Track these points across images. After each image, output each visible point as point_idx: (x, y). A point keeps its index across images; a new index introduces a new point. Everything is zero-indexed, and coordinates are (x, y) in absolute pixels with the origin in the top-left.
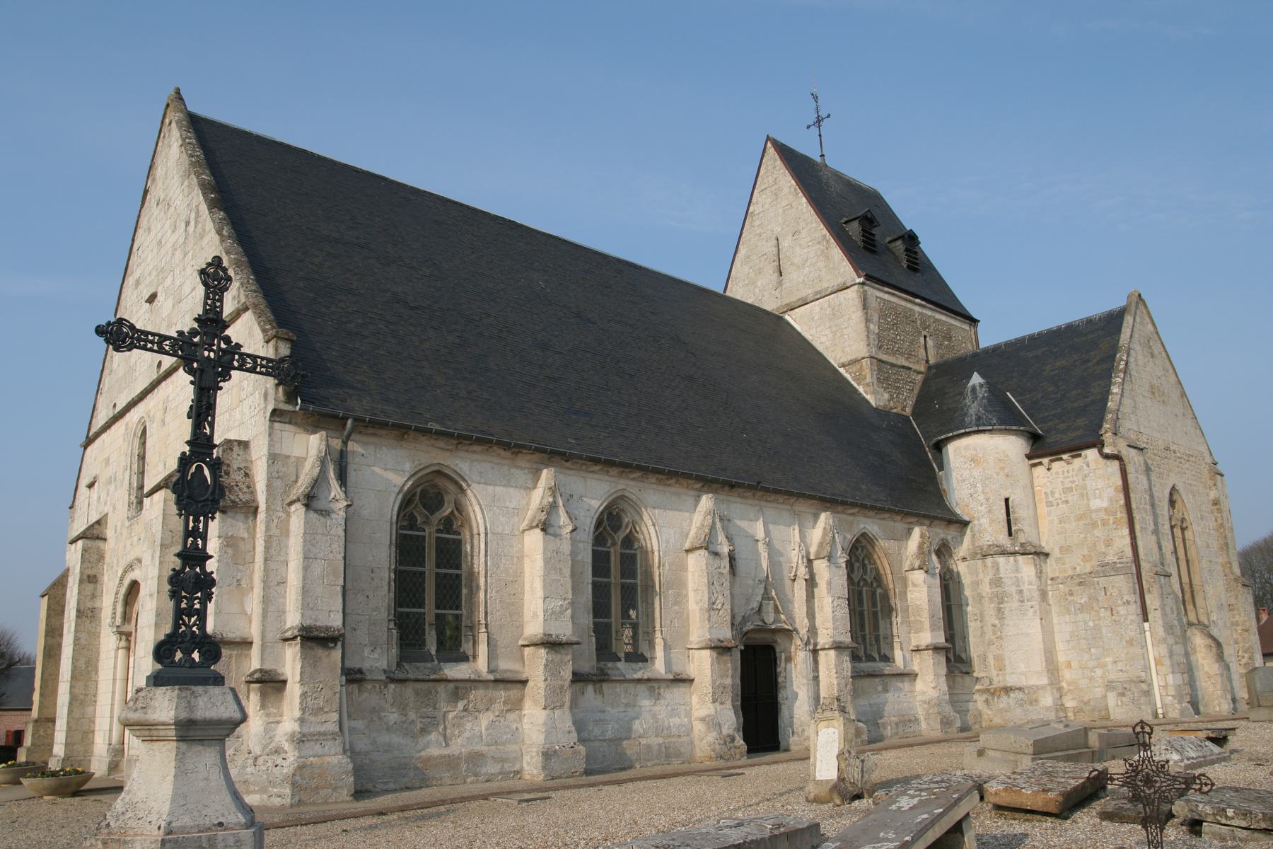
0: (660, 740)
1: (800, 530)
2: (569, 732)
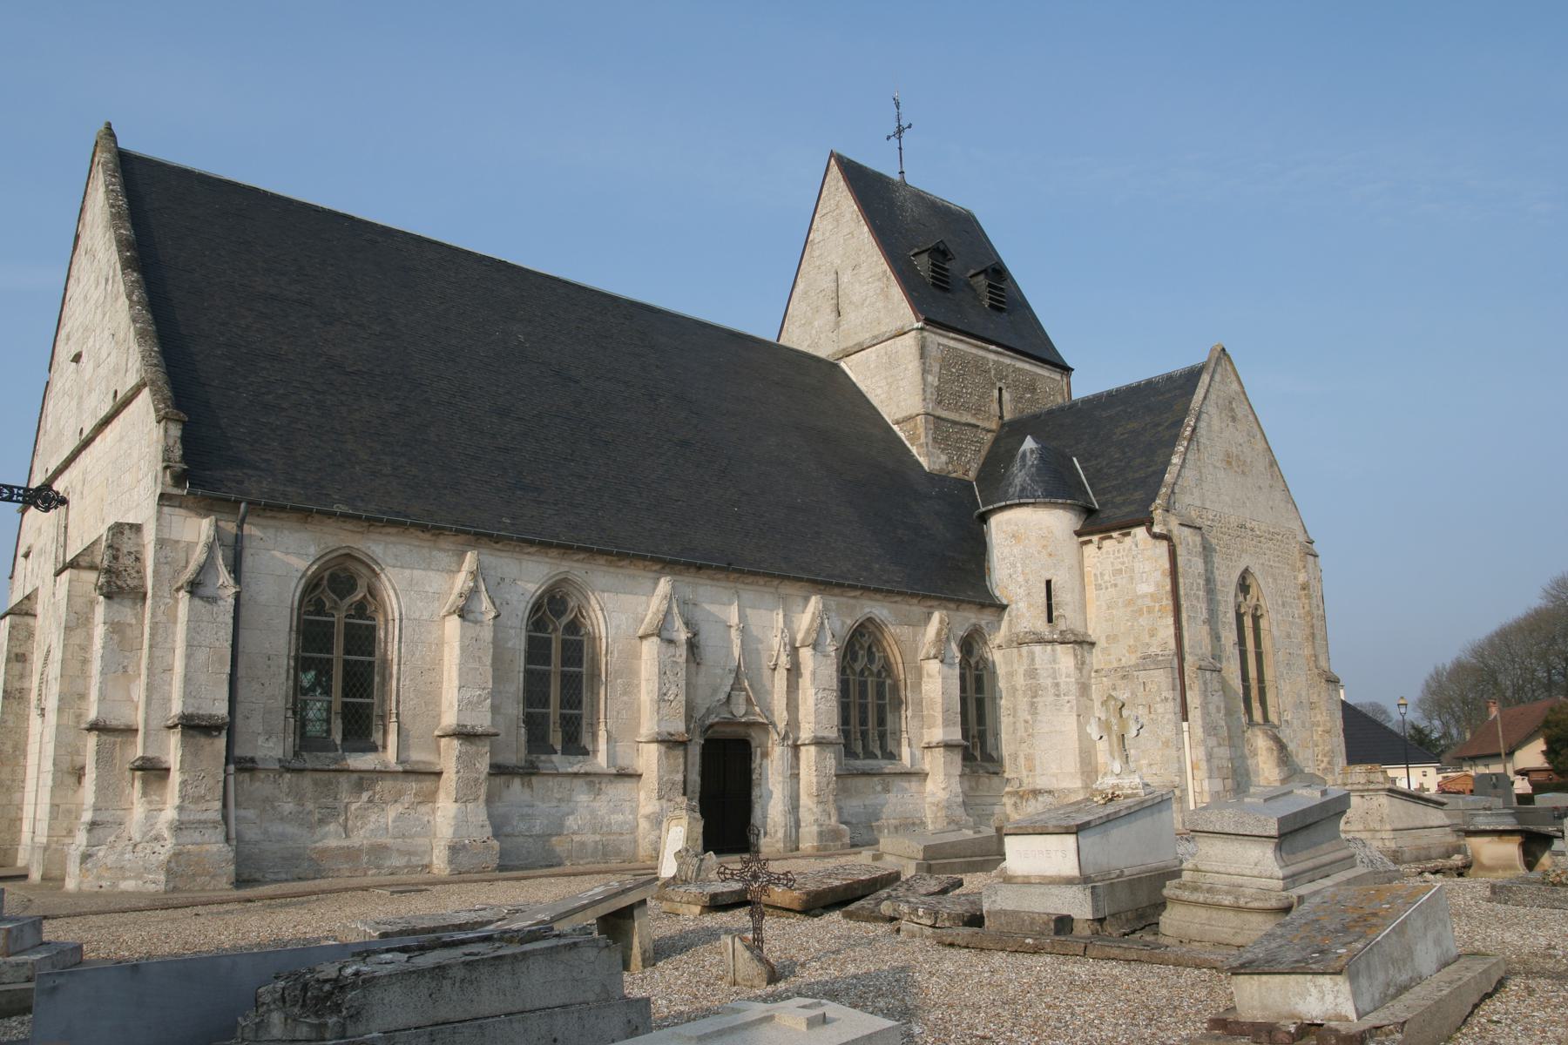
0: (598, 838)
1: (785, 616)
2: (482, 826)
